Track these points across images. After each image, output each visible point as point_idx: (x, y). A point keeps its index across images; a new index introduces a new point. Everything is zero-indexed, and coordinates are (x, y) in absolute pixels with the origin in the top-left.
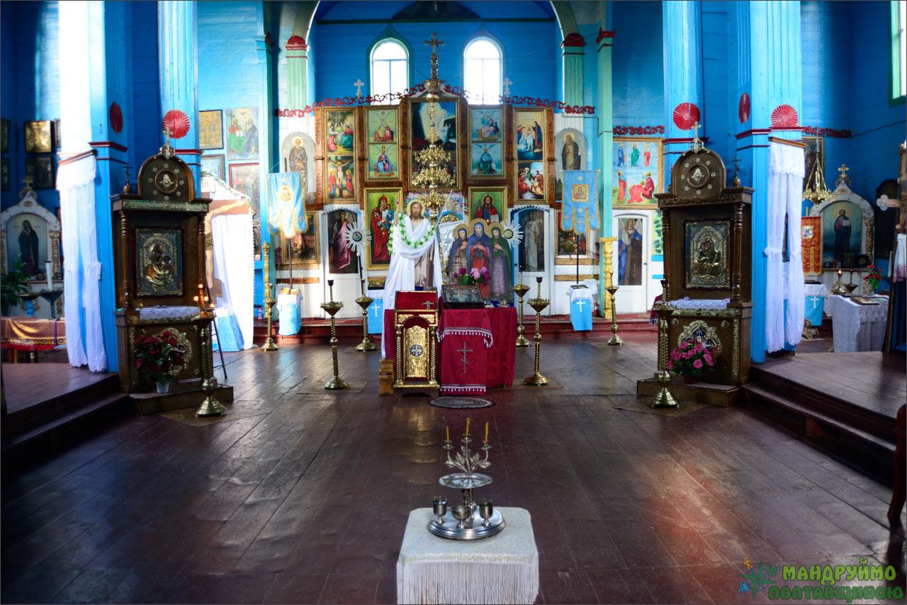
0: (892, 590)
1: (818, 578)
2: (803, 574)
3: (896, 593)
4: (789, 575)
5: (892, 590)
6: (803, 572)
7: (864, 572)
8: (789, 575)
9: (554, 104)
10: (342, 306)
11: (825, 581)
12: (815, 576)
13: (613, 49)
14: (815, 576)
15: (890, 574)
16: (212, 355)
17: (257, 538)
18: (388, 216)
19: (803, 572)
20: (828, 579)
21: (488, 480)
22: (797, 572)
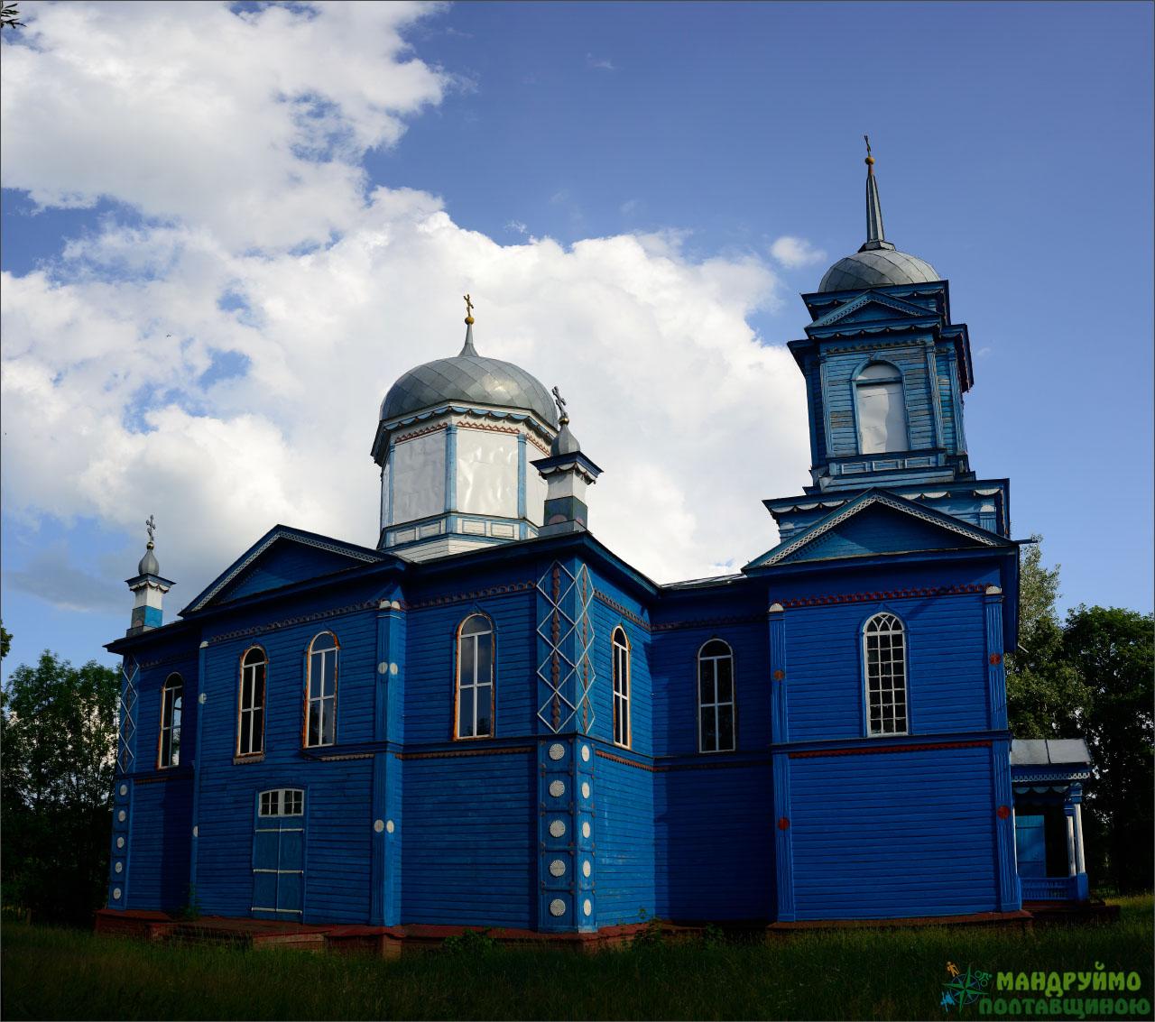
0: (1136, 1003)
1: (1042, 988)
2: (1043, 1008)
3: (1141, 1007)
4: (1005, 984)
5: (1136, 1003)
6: (1022, 980)
7: (1100, 980)
8: (1005, 984)
9: (575, 735)
10: (1042, 539)
11: (1051, 992)
12: (1038, 985)
13: (769, 736)
14: (1038, 985)
15: (1134, 982)
16: (769, 763)
17: (610, 941)
18: (1029, 558)
19: (1022, 980)
20: (1054, 989)
21: (961, 471)
22: (1015, 979)
